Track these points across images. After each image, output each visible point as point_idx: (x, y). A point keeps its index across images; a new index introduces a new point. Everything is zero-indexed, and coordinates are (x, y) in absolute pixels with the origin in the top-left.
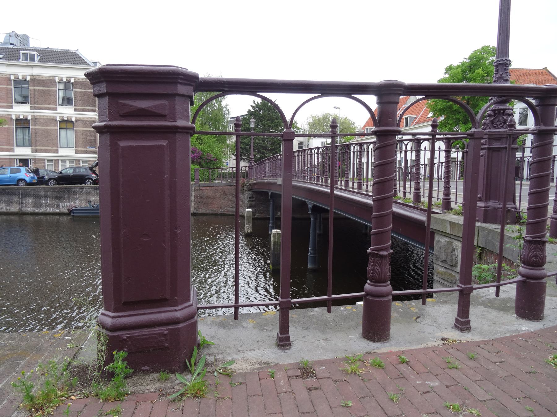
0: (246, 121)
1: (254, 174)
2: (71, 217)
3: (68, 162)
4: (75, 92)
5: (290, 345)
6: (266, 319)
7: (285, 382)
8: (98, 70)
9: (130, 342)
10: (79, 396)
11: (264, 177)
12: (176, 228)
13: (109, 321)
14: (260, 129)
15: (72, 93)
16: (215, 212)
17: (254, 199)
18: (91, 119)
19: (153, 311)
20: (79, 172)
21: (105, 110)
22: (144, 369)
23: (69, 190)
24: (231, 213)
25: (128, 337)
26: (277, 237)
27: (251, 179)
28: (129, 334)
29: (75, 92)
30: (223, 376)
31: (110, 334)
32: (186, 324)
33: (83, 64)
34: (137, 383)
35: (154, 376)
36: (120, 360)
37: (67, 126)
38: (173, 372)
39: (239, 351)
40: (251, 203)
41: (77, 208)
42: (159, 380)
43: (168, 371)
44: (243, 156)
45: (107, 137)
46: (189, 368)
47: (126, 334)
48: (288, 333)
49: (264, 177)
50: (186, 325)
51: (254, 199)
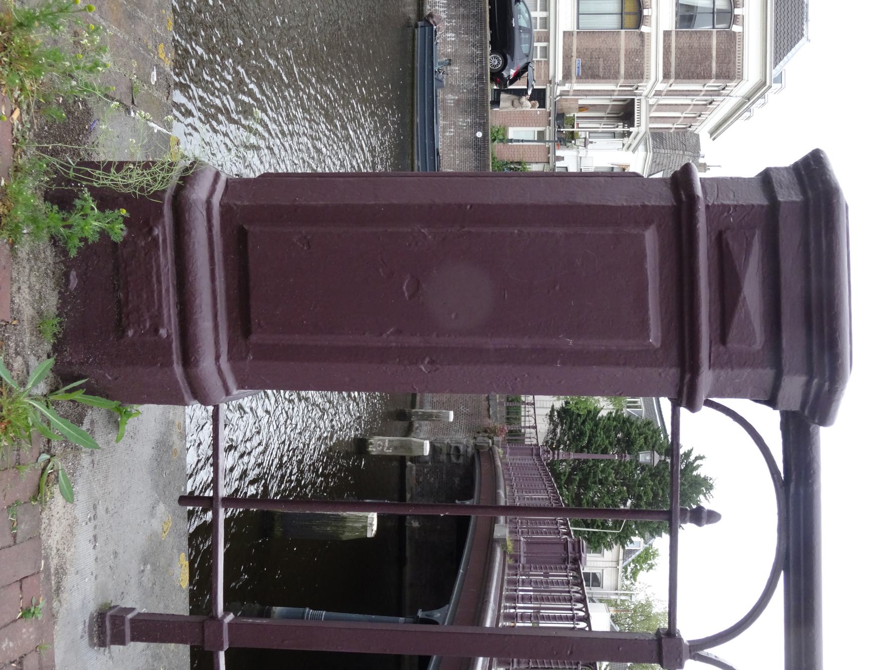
0: (652, 438)
1: (519, 460)
2: (413, 22)
3: (544, 14)
4: (709, 34)
5: (100, 646)
6: (169, 565)
7: (9, 653)
8: (834, 185)
9: (143, 243)
10: (20, 127)
11: (512, 486)
12: (432, 362)
13: (200, 195)
14: (632, 472)
15: (708, 28)
17: (454, 459)
18: (646, 68)
19: (218, 301)
20: (520, 39)
21: (732, 197)
22: (71, 277)
23: (480, 20)
25: (155, 240)
26: (356, 525)
27: (505, 453)
28: (164, 240)
29: (709, 34)
30: (36, 479)
31: (168, 196)
32: (181, 384)
33: (776, 53)
34: (36, 259)
35: (52, 301)
36: (103, 225)
37: (629, 14)
38: (57, 349)
39: (95, 507)
40: (445, 451)
41: (436, 35)
42: (40, 313)
43: (61, 336)
44: (562, 429)
45: (665, 199)
46: (64, 386)
47: (164, 234)
48: (133, 639)
49: (512, 486)
50: (177, 382)
51: (454, 459)
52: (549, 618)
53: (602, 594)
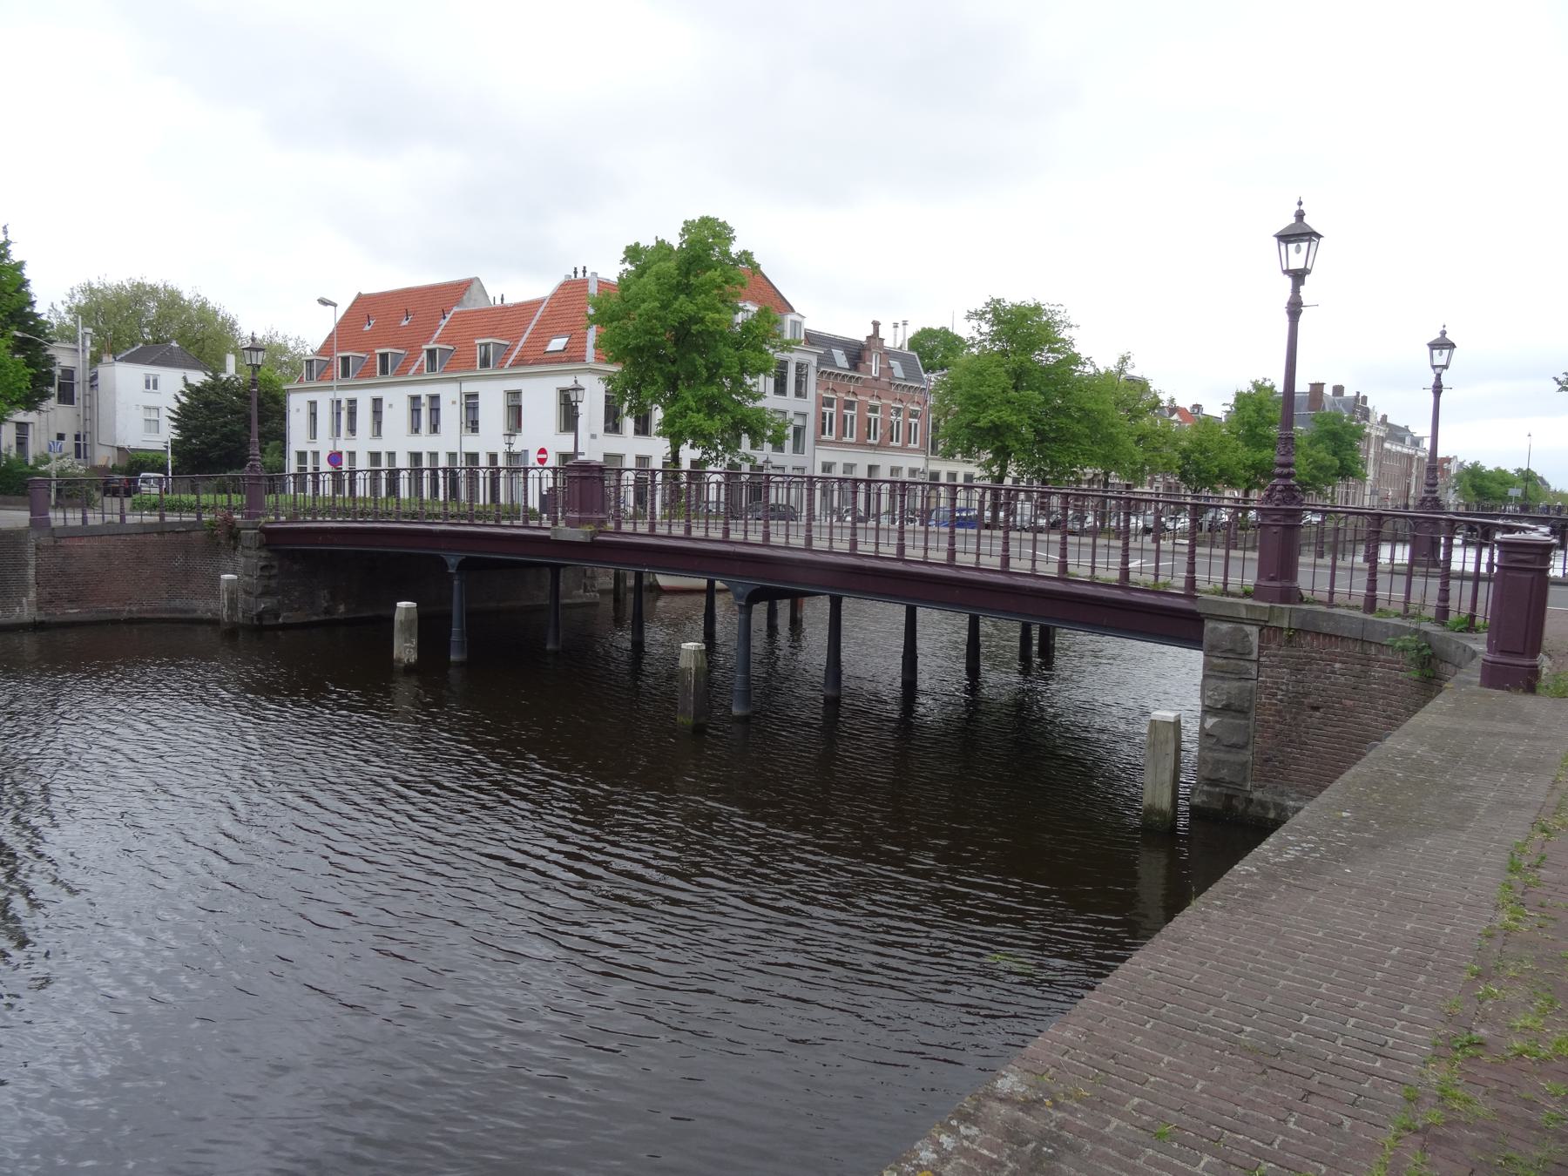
16: (109, 617)
17: (274, 572)
24: (164, 616)
51: (274, 572)
52: (1474, 607)
53: (84, 370)
